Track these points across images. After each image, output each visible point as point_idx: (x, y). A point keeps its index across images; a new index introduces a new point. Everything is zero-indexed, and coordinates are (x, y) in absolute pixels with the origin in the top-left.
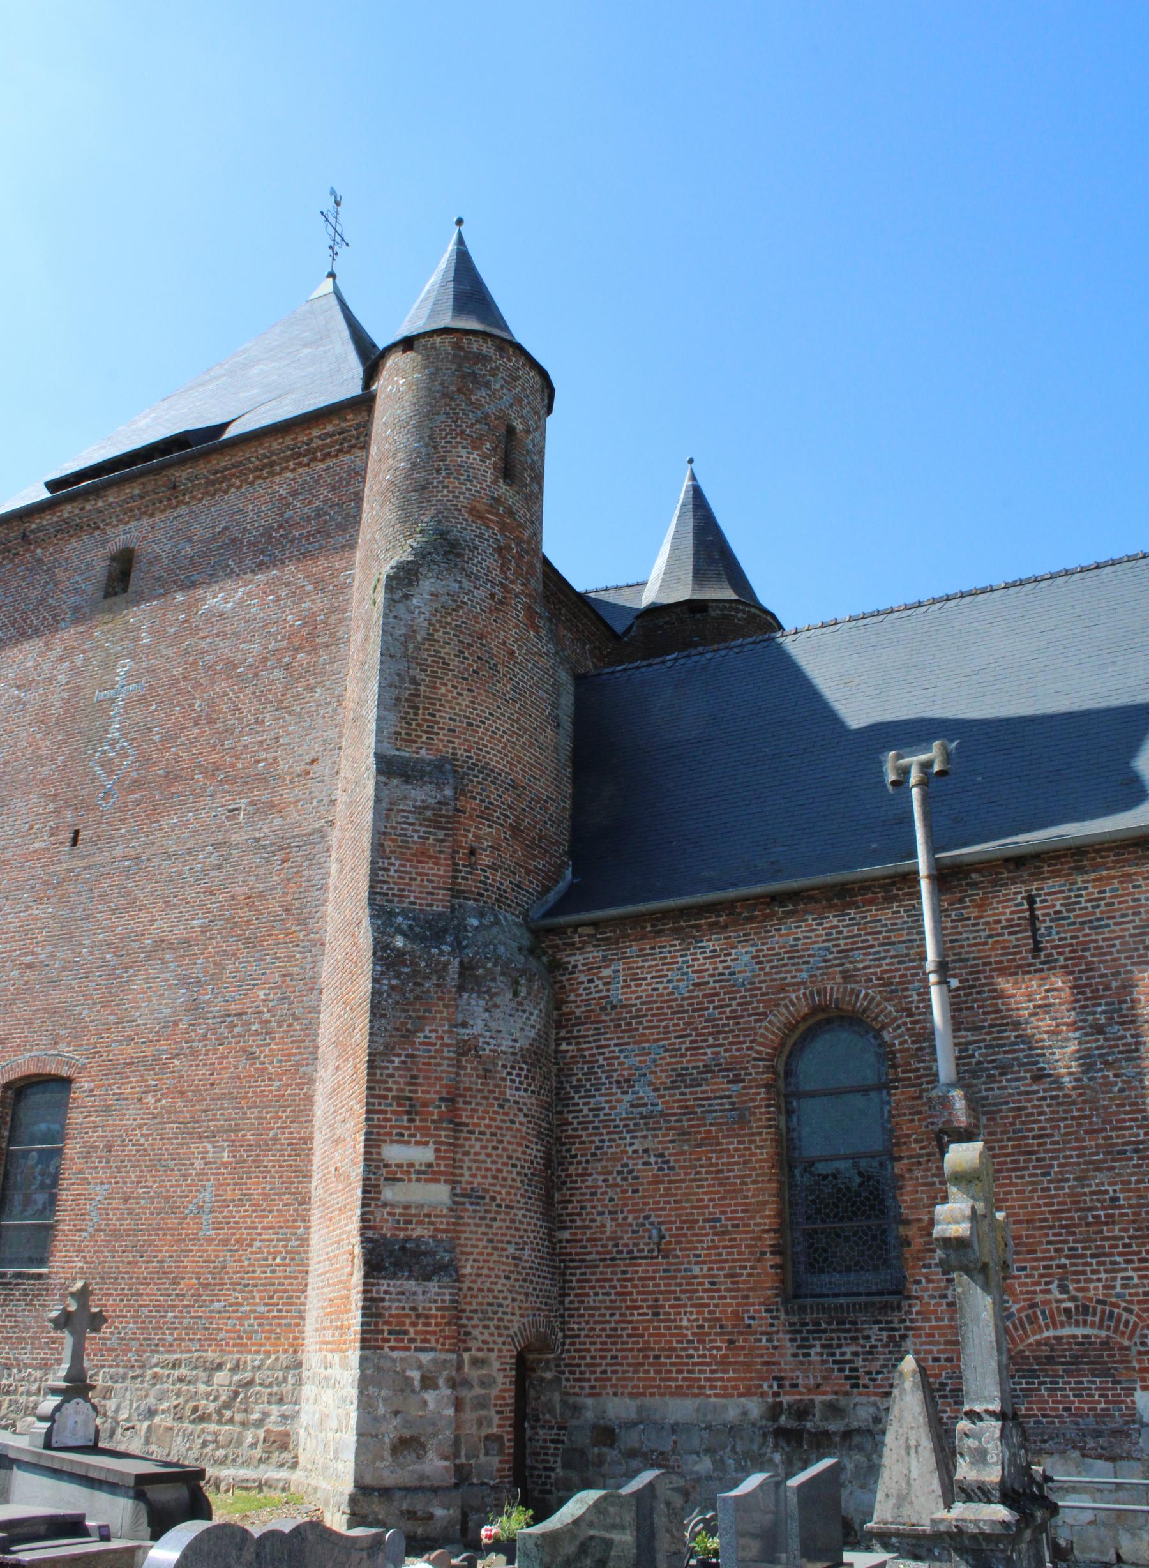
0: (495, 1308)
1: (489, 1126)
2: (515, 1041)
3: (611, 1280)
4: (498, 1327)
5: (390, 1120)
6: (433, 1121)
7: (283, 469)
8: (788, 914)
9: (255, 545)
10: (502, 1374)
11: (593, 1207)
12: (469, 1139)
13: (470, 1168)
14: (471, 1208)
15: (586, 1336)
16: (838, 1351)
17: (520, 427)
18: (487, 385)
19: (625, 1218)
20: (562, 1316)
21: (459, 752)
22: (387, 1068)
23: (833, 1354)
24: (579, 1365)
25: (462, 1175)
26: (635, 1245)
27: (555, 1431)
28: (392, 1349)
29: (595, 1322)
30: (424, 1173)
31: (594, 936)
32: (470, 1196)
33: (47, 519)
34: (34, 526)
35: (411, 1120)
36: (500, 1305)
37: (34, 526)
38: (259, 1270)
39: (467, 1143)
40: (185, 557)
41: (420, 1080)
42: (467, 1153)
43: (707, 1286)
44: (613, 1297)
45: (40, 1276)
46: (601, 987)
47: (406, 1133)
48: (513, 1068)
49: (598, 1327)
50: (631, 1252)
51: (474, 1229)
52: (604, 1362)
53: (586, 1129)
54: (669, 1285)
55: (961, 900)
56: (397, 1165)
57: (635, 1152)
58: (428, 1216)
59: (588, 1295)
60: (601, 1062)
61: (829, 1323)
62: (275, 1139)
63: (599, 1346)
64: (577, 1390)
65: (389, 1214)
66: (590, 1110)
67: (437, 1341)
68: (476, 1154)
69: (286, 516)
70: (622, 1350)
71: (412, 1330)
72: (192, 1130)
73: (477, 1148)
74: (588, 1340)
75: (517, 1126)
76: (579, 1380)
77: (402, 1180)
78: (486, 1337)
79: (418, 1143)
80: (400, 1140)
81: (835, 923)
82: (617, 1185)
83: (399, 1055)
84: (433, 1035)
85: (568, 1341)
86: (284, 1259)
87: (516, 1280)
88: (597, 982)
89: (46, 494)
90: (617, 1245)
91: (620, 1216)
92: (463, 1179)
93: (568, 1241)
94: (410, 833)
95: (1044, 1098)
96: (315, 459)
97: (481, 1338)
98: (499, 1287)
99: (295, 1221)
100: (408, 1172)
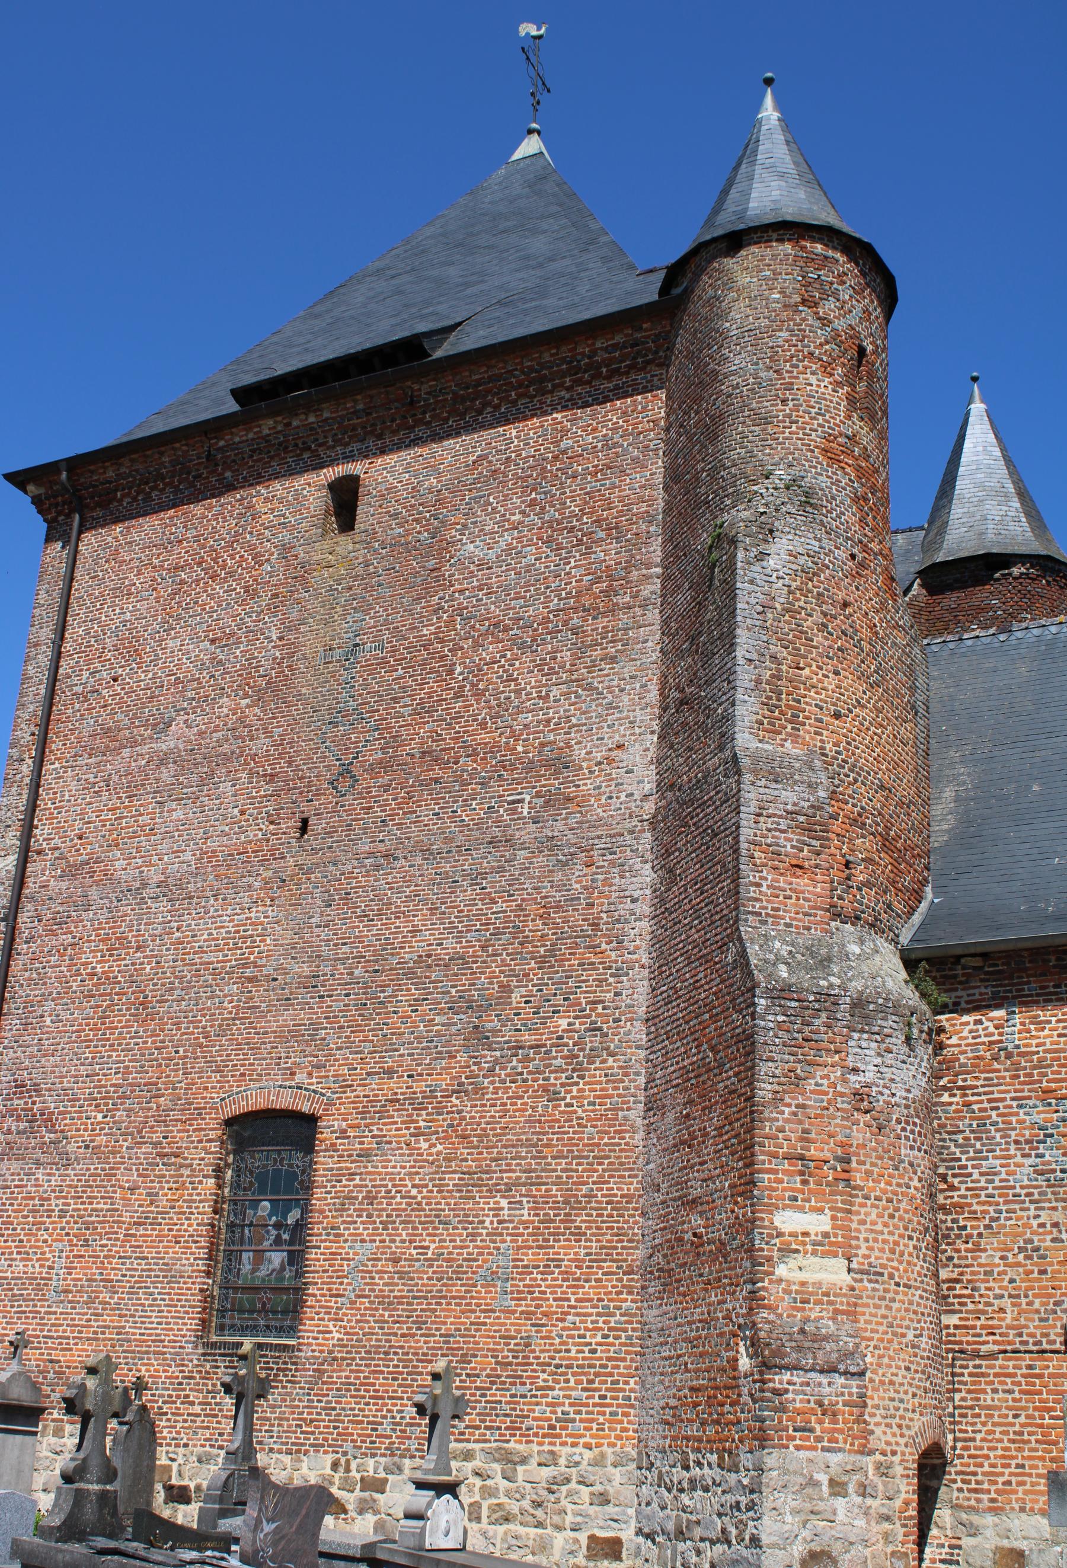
0: (896, 1404)
1: (885, 1192)
3: (1015, 1375)
4: (900, 1426)
5: (781, 1181)
6: (828, 1184)
7: (555, 387)
9: (524, 479)
10: (905, 1481)
11: (988, 1289)
12: (865, 1205)
13: (867, 1240)
14: (870, 1286)
15: (983, 1440)
17: (870, 348)
18: (835, 294)
20: (952, 1415)
21: (828, 746)
22: (777, 1120)
24: (975, 1474)
25: (858, 1247)
26: (1044, 1335)
27: (947, 1549)
28: (798, 1448)
29: (994, 1424)
30: (820, 1244)
31: (980, 968)
33: (239, 436)
34: (222, 443)
35: (805, 1182)
36: (901, 1401)
37: (222, 443)
38: (574, 1349)
39: (863, 1210)
40: (430, 490)
41: (813, 1136)
42: (863, 1222)
44: (1017, 1395)
45: (286, 1348)
46: (992, 1029)
47: (800, 1196)
48: (907, 1123)
49: (998, 1429)
50: (1040, 1343)
51: (873, 1311)
52: (1007, 1471)
53: (978, 1196)
54: (974, 1383)
56: (791, 1235)
57: (1042, 1225)
58: (827, 1294)
59: (984, 1392)
60: (994, 1118)
62: (590, 1196)
63: (1000, 1452)
64: (973, 1502)
65: (785, 1291)
66: (981, 1174)
67: (845, 1442)
68: (874, 1223)
69: (563, 445)
70: (1030, 1458)
71: (818, 1427)
72: (475, 1182)
73: (874, 1216)
74: (985, 1445)
75: (912, 1190)
76: (976, 1491)
77: (797, 1251)
78: (889, 1437)
79: (813, 1209)
80: (792, 1202)
82: (1018, 1264)
83: (789, 1105)
84: (825, 1082)
85: (959, 1445)
86: (605, 1337)
87: (916, 1371)
88: (986, 1024)
89: (231, 406)
90: (1020, 1335)
91: (1024, 1301)
92: (860, 1252)
93: (956, 1327)
94: (782, 842)
96: (598, 376)
97: (883, 1438)
99: (618, 1293)
100: (804, 1244)
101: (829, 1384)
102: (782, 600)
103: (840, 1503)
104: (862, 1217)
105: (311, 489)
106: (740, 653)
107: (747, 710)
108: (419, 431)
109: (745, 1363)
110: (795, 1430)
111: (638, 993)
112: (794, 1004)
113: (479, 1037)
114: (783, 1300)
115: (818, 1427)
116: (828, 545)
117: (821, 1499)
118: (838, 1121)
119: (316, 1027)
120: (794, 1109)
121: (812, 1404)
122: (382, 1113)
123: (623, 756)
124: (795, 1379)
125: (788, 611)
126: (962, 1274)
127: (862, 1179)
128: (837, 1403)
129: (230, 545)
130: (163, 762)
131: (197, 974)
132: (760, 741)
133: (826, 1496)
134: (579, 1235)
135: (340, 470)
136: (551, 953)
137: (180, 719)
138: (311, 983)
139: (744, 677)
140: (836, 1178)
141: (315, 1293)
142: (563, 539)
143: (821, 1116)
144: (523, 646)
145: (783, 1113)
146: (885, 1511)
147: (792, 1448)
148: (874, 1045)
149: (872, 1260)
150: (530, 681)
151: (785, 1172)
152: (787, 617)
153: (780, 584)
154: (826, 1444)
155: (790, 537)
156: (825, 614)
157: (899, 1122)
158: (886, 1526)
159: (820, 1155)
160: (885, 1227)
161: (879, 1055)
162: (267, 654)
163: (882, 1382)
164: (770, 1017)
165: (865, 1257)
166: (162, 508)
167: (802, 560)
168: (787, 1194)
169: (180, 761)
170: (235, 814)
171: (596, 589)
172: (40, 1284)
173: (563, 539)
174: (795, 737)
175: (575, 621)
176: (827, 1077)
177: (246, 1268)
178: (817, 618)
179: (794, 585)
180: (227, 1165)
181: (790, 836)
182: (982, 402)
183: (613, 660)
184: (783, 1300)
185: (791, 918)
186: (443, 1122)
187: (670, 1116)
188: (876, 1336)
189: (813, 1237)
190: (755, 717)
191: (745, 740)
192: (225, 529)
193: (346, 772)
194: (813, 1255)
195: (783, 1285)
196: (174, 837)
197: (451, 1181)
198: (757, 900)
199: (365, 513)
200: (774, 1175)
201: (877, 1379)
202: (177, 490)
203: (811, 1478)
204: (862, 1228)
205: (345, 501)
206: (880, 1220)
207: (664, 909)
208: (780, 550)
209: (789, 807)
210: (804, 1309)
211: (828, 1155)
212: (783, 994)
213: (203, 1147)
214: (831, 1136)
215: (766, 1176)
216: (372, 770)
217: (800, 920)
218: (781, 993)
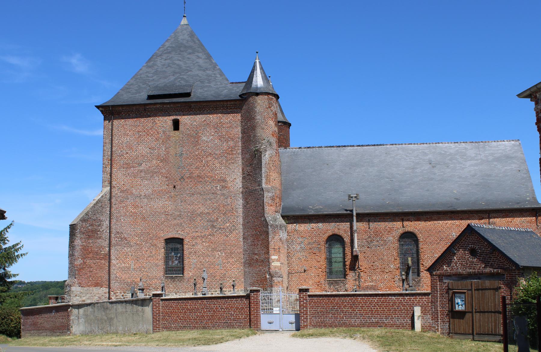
72: (214, 250)
105: (168, 120)
106: (263, 172)
107: (264, 181)
108: (191, 112)
109: (268, 276)
111: (241, 220)
113: (213, 226)
119: (181, 224)
122: (196, 238)
123: (236, 180)
129: (151, 129)
130: (141, 172)
131: (155, 213)
134: (233, 258)
135: (175, 117)
136: (225, 213)
137: (144, 163)
138: (180, 216)
139: (263, 175)
140: (278, 251)
141: (186, 268)
142: (222, 139)
144: (216, 158)
150: (218, 165)
160: (284, 258)
162: (163, 153)
166: (133, 118)
169: (146, 172)
170: (158, 183)
171: (229, 150)
172: (129, 268)
173: (222, 139)
175: (226, 155)
177: (170, 264)
183: (233, 163)
186: (208, 240)
187: (249, 241)
191: (264, 186)
192: (150, 125)
193: (182, 178)
194: (277, 262)
196: (146, 187)
197: (210, 250)
199: (181, 127)
200: (271, 251)
202: (136, 114)
205: (176, 125)
207: (244, 207)
208: (268, 153)
213: (161, 244)
216: (187, 178)
218: (272, 225)
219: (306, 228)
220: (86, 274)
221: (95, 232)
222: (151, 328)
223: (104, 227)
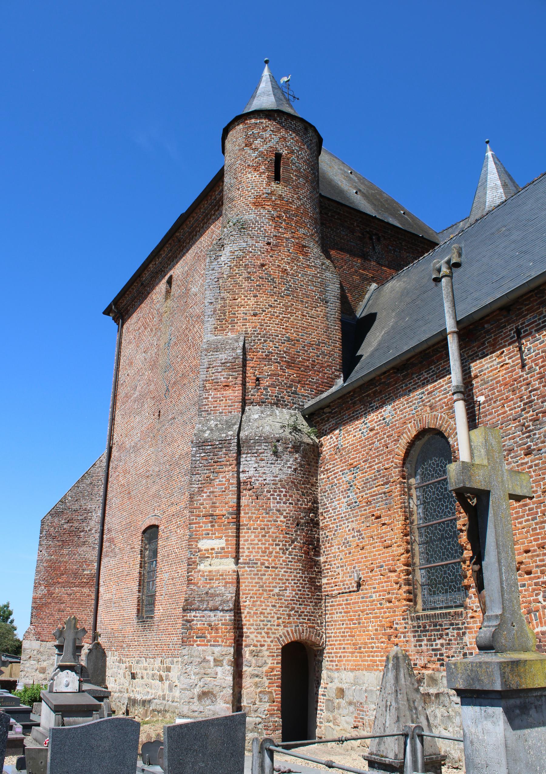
2: (276, 477)
5: (202, 527)
8: (405, 377)
10: (271, 658)
13: (248, 548)
14: (248, 569)
16: (434, 643)
19: (346, 569)
21: (249, 330)
22: (200, 500)
23: (432, 645)
28: (198, 645)
32: (248, 563)
35: (212, 526)
39: (246, 535)
41: (218, 504)
43: (379, 606)
47: (211, 532)
51: (250, 581)
55: (483, 344)
56: (207, 550)
58: (222, 575)
61: (430, 626)
65: (201, 576)
67: (223, 642)
71: (208, 636)
73: (253, 537)
77: (208, 557)
78: (259, 638)
79: (217, 538)
81: (426, 376)
83: (206, 493)
84: (224, 479)
95: (531, 467)
97: (255, 639)
98: (268, 611)
101: (215, 616)
102: (227, 273)
103: (219, 669)
104: (246, 538)
110: (197, 638)
112: (209, 447)
114: (200, 579)
115: (208, 636)
116: (250, 242)
117: (210, 668)
118: (230, 496)
120: (208, 494)
121: (206, 625)
124: (197, 614)
125: (229, 277)
126: (327, 558)
127: (246, 521)
128: (219, 624)
132: (216, 336)
133: (212, 666)
143: (222, 495)
145: (203, 496)
146: (256, 672)
147: (195, 646)
148: (254, 459)
149: (252, 557)
151: (203, 523)
152: (229, 279)
153: (226, 266)
154: (212, 643)
155: (231, 245)
156: (249, 273)
157: (268, 492)
158: (257, 679)
159: (221, 513)
161: (257, 462)
163: (255, 613)
164: (198, 455)
165: (247, 556)
167: (236, 253)
168: (204, 533)
174: (232, 330)
176: (225, 477)
178: (245, 275)
179: (232, 265)
180: (146, 549)
181: (223, 373)
182: (491, 151)
184: (200, 579)
185: (222, 409)
188: (252, 592)
189: (216, 550)
190: (213, 326)
195: (201, 573)
198: (206, 405)
201: (252, 612)
203: (205, 658)
204: (246, 543)
206: (256, 539)
209: (223, 361)
210: (210, 583)
211: (224, 512)
212: (204, 444)
214: (226, 504)
215: (194, 526)
217: (227, 409)
219: (358, 434)
220: (52, 615)
221: (75, 533)
222: (277, 736)
223: (92, 523)
